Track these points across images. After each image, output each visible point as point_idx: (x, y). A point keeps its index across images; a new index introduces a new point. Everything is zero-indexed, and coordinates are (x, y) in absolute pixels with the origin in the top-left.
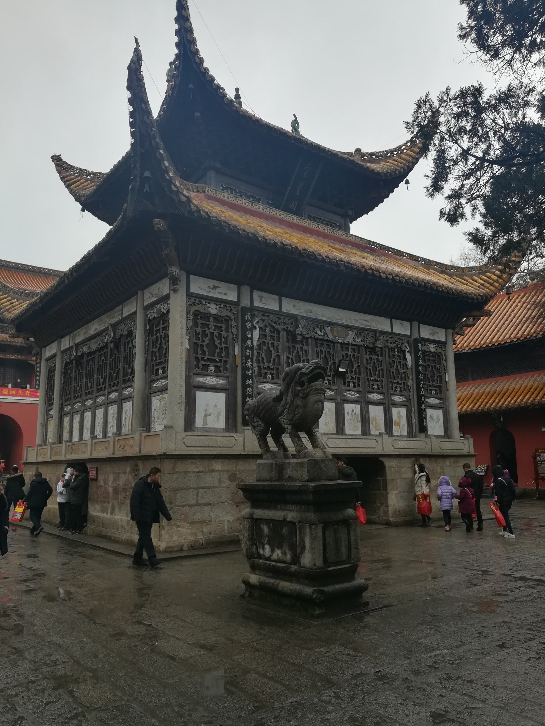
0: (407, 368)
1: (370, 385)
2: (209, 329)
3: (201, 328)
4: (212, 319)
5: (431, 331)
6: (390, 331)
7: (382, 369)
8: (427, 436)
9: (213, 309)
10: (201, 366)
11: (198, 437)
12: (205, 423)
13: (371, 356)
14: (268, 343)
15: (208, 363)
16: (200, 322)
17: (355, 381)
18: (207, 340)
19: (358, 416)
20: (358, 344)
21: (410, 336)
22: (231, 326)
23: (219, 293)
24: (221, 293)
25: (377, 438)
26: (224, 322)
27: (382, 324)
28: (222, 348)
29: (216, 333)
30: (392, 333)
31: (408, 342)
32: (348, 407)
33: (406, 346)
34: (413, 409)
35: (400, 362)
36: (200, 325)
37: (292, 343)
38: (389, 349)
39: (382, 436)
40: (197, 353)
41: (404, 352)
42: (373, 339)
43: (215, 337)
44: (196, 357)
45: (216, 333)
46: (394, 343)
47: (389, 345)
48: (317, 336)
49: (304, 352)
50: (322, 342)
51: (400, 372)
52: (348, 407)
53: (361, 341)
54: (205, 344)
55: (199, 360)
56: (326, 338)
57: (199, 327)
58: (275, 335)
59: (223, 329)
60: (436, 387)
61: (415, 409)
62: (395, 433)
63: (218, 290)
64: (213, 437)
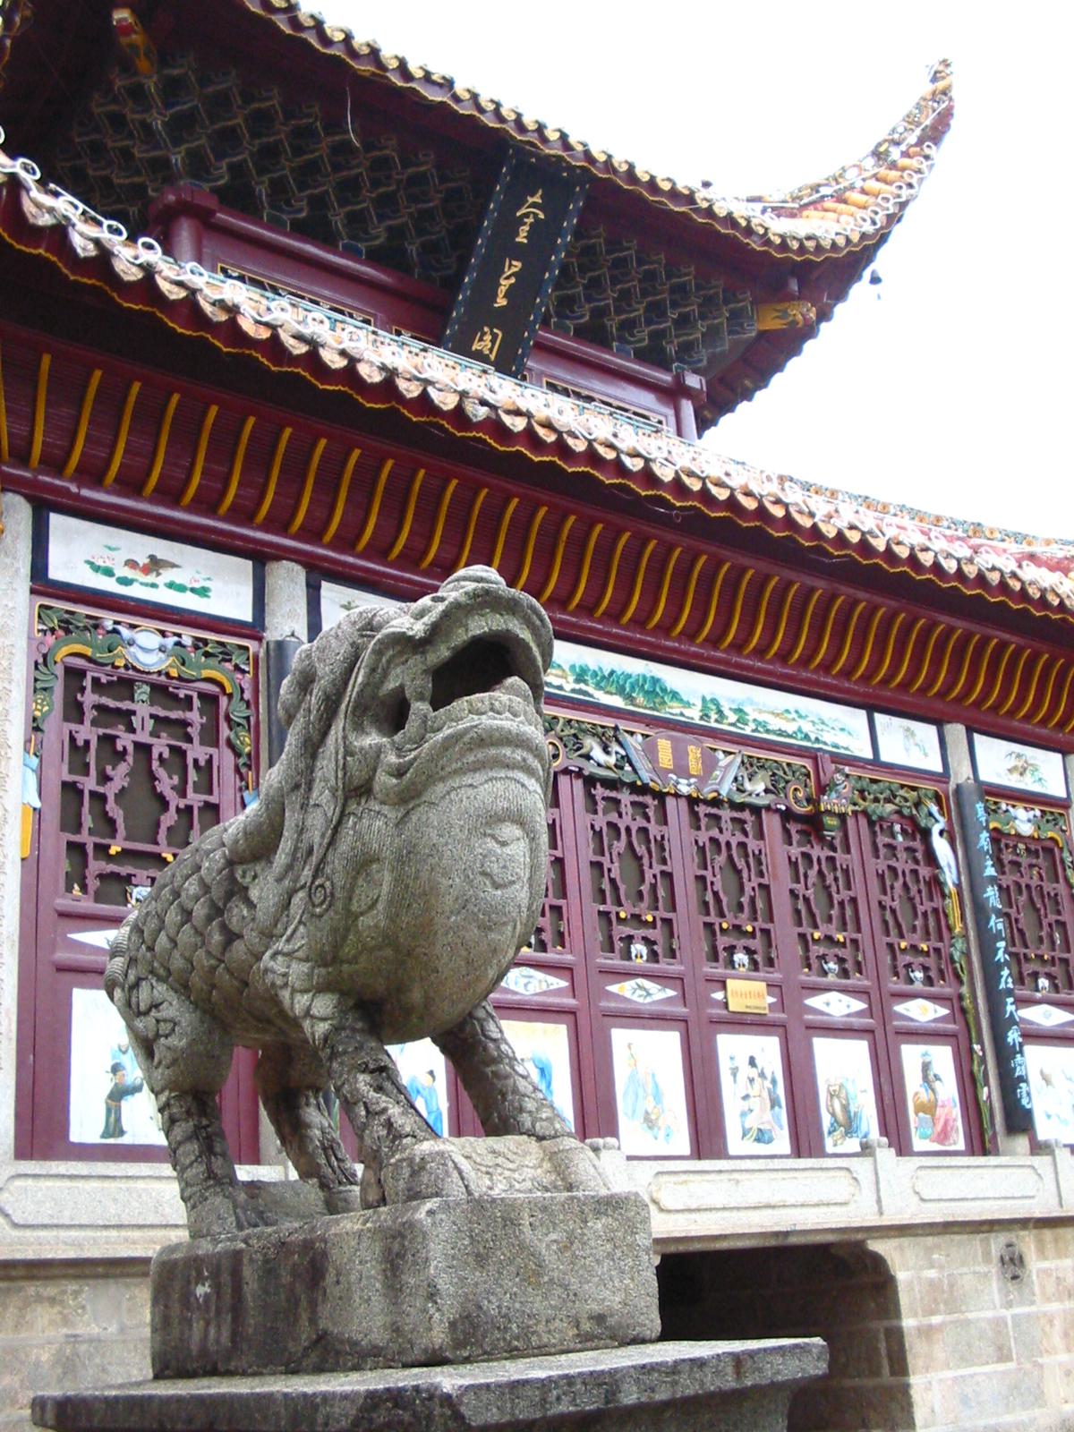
0: (944, 896)
1: (814, 961)
2: (133, 731)
3: (94, 723)
4: (143, 692)
5: (1013, 762)
6: (869, 755)
7: (854, 900)
8: (1038, 1148)
9: (148, 649)
10: (93, 884)
11: (67, 1183)
12: (114, 1127)
13: (805, 849)
14: (628, 829)
15: (124, 870)
16: (89, 698)
17: (756, 944)
18: (120, 775)
19: (774, 1082)
20: (753, 800)
21: (944, 777)
22: (228, 719)
23: (171, 585)
24: (181, 588)
25: (854, 1163)
26: (196, 703)
27: (839, 727)
28: (189, 809)
29: (161, 746)
30: (876, 762)
31: (937, 799)
32: (731, 1048)
33: (930, 814)
34: (977, 1047)
35: (914, 872)
36: (90, 714)
37: (800, 844)
38: (871, 824)
39: (872, 1154)
40: (78, 828)
41: (926, 834)
42: (812, 783)
43: (155, 764)
44: (799, 934)
45: (161, 746)
46: (888, 801)
47: (871, 807)
48: (590, 768)
49: (839, 874)
50: (714, 811)
51: (920, 909)
52: (731, 1048)
53: (767, 791)
54: (110, 790)
55: (85, 855)
56: (627, 775)
57: (87, 722)
58: (917, 844)
59: (194, 731)
60: (1053, 961)
61: (984, 1048)
62: (919, 1144)
63: (168, 575)
64: (140, 1184)
